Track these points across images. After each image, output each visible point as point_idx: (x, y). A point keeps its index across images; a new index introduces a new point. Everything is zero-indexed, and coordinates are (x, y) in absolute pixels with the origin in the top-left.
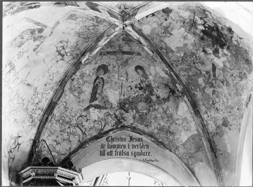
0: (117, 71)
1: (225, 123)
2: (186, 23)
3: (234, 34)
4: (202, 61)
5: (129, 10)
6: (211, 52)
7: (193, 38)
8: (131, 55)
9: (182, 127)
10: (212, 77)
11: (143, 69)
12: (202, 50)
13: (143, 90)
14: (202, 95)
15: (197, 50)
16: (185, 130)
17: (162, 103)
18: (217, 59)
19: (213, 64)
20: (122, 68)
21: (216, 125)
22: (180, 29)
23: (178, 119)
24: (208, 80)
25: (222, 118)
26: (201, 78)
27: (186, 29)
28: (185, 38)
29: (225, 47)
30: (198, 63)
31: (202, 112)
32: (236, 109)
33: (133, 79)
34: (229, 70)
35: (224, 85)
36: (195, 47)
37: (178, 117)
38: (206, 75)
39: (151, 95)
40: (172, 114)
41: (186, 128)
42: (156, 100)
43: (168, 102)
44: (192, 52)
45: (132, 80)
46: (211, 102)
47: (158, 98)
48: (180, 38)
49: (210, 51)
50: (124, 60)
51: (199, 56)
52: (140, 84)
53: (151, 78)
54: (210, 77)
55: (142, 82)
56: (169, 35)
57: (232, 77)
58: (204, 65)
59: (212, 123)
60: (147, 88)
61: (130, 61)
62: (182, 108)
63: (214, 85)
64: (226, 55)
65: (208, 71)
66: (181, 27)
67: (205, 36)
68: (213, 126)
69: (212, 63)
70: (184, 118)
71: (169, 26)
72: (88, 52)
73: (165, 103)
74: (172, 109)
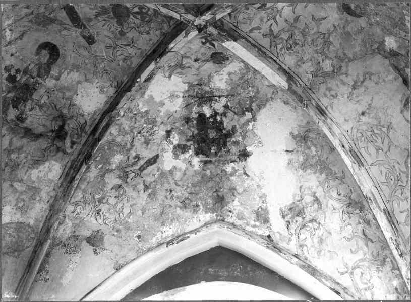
0: (21, 15)
1: (95, 240)
2: (200, 87)
3: (243, 162)
4: (150, 140)
5: (229, 20)
6: (176, 142)
7: (179, 107)
8: (71, 24)
9: (16, 198)
10: (136, 167)
11: (56, 60)
12: (169, 129)
13: (11, 85)
14: (96, 177)
15: (162, 123)
16: (16, 205)
17: (19, 134)
18: (171, 157)
19: (157, 156)
20: (31, 21)
21: (75, 231)
22: (184, 83)
23: (21, 181)
24: (127, 166)
25: (96, 229)
26: (122, 156)
27: (188, 90)
28: (173, 96)
29: (202, 157)
30: (143, 136)
31: (73, 199)
32: (137, 234)
33: (18, 54)
34: (172, 182)
35: (144, 191)
36: (167, 118)
37: (26, 178)
38: (131, 158)
39: (13, 106)
40: (18, 165)
41: (20, 205)
42: (12, 120)
43: (31, 141)
44: (155, 119)
45: (16, 53)
46: (99, 197)
47: (18, 120)
48: (168, 91)
49: (176, 139)
50: (52, 15)
51: (155, 131)
52: (18, 71)
53: (50, 83)
54: (133, 164)
55: (26, 72)
56: (167, 75)
57: (168, 194)
58: (144, 146)
59: (70, 224)
60: (21, 87)
61: (55, 27)
62: (46, 169)
63: (129, 180)
64: (190, 164)
65: (140, 156)
66: (189, 83)
67: (195, 122)
68: (68, 231)
69: (158, 154)
70: (35, 187)
71: (184, 67)
72: (290, 85)
73: (22, 138)
74: (26, 157)
